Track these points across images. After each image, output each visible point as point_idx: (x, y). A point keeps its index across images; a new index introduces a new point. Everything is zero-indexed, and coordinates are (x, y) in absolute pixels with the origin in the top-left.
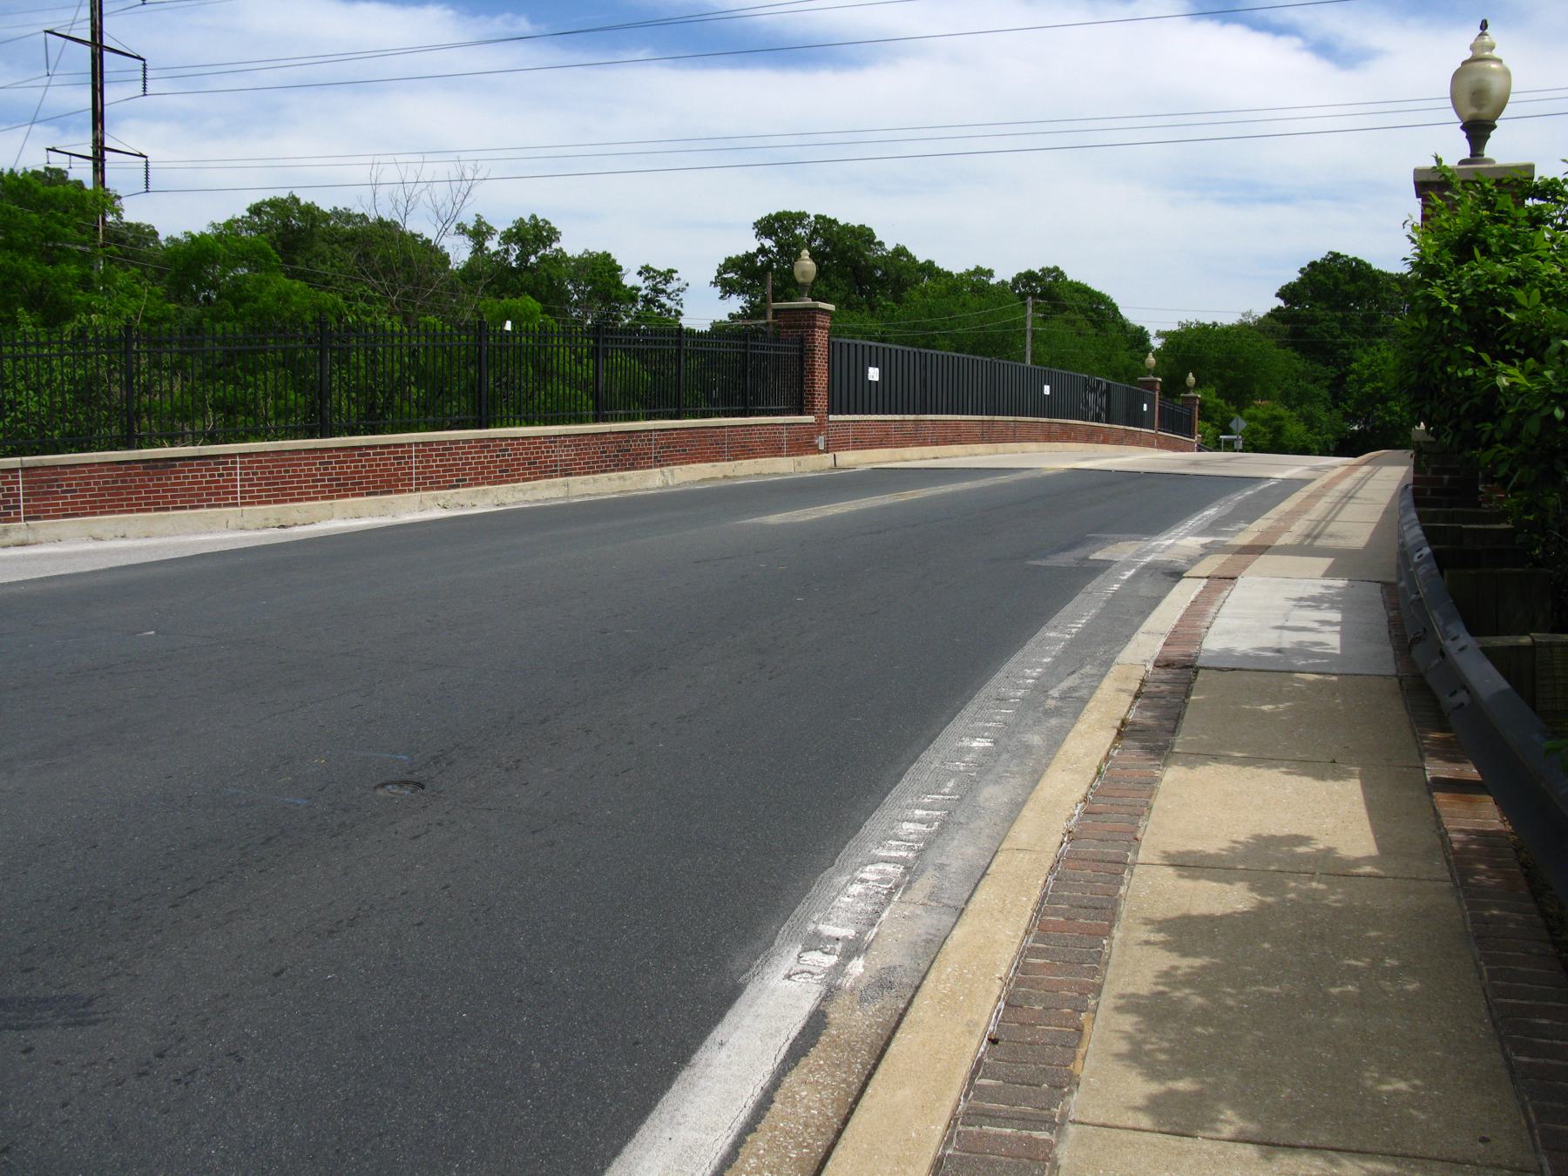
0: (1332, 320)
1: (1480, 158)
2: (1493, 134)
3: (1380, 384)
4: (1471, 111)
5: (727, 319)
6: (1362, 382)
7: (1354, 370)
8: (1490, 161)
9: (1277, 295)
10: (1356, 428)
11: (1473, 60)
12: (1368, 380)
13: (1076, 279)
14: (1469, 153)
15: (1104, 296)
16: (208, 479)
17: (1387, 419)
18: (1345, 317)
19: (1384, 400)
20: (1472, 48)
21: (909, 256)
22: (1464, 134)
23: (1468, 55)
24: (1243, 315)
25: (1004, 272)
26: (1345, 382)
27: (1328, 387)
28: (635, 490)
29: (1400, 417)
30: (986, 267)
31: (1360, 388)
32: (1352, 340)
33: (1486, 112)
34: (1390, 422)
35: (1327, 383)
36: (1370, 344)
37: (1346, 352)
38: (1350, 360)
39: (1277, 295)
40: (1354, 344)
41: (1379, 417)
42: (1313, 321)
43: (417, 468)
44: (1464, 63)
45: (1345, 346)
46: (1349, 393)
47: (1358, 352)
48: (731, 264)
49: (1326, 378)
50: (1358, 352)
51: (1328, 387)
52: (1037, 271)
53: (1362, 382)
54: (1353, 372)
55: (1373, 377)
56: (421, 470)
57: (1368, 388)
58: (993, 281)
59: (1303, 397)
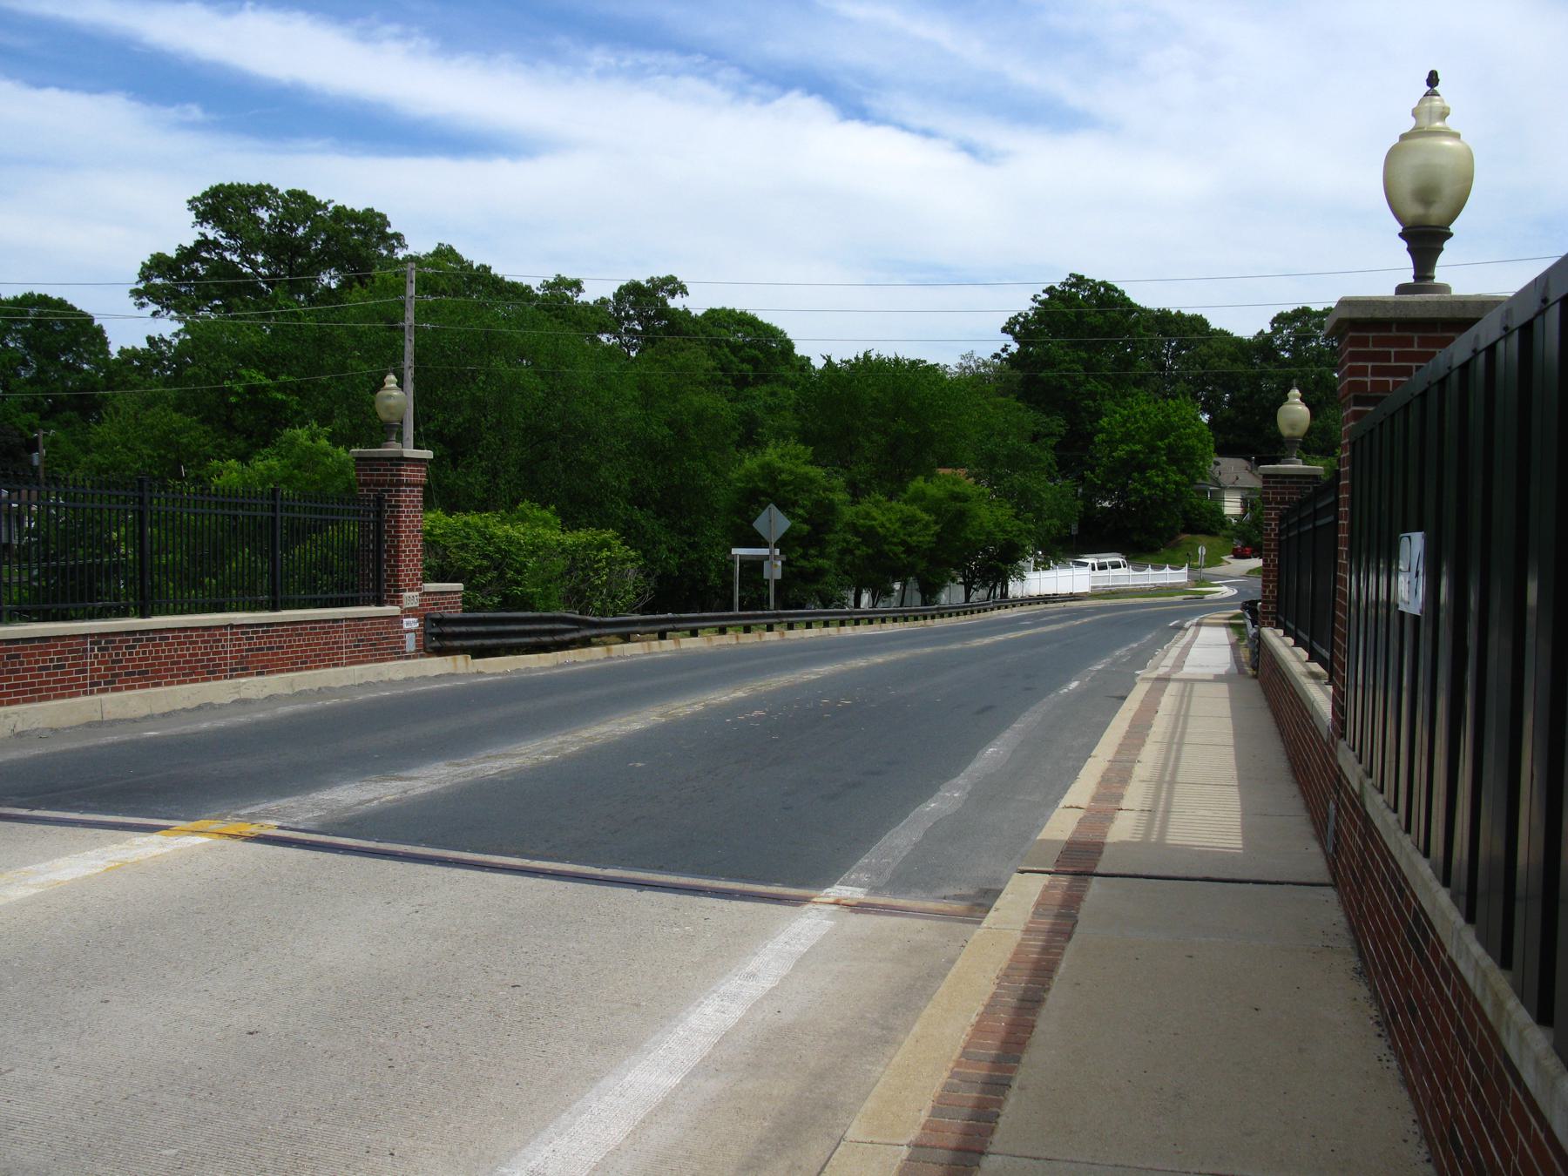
0: (1072, 361)
1: (1428, 283)
2: (1447, 245)
3: (1138, 447)
4: (1414, 210)
5: (146, 346)
6: (1112, 443)
7: (1103, 428)
8: (1444, 288)
9: (1004, 330)
10: (1106, 504)
11: (1416, 133)
12: (1122, 441)
13: (845, 352)
14: (1412, 272)
15: (775, 329)
16: (10, 667)
17: (1146, 493)
18: (1090, 358)
19: (1142, 468)
20: (1415, 113)
21: (458, 259)
22: (1404, 245)
23: (1409, 124)
24: (963, 357)
25: (597, 289)
26: (1093, 443)
27: (1054, 448)
28: (588, 662)
29: (1163, 490)
30: (570, 275)
31: (1111, 452)
32: (1101, 388)
33: (1436, 214)
34: (1150, 497)
35: (1053, 441)
36: (1124, 396)
37: (1091, 403)
38: (1098, 415)
39: (1004, 330)
40: (1103, 394)
41: (1137, 491)
42: (1050, 363)
43: (226, 640)
44: (1403, 137)
45: (1092, 395)
46: (1098, 459)
47: (1109, 405)
48: (159, 264)
49: (1052, 434)
50: (1109, 405)
51: (1054, 448)
52: (644, 283)
53: (1112, 443)
54: (1102, 430)
55: (1128, 437)
56: (223, 638)
57: (1121, 452)
58: (582, 298)
59: (1016, 460)
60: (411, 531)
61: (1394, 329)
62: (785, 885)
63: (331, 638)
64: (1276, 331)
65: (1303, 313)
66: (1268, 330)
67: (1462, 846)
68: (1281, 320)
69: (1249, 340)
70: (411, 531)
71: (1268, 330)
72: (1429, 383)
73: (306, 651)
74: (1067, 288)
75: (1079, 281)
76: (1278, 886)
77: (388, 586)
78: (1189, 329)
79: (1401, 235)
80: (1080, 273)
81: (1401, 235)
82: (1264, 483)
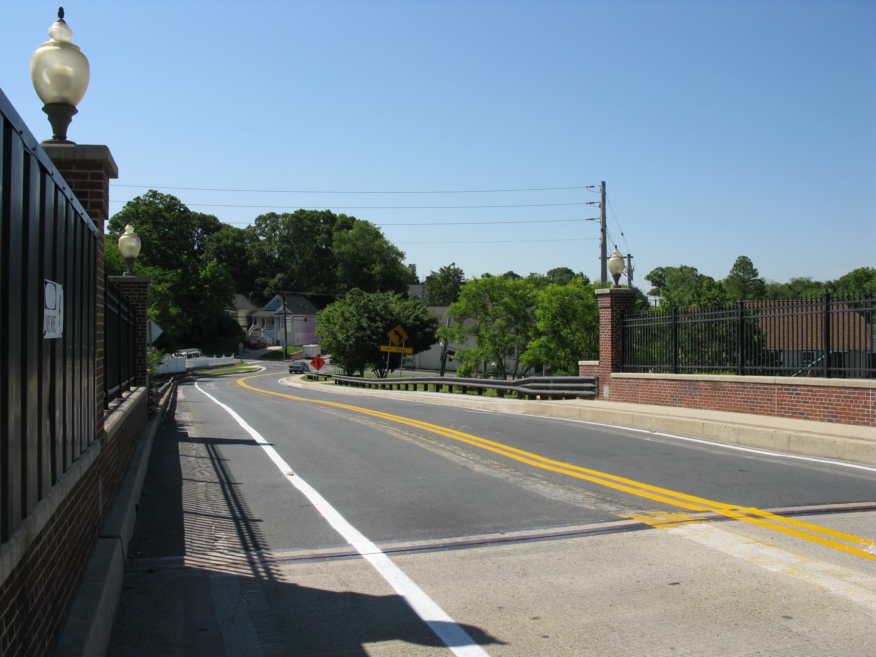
22: (46, 116)
60: (605, 346)
61: (89, 192)
62: (8, 611)
63: (721, 393)
64: (259, 225)
65: (273, 215)
66: (253, 225)
67: (399, 419)
68: (261, 219)
69: (244, 230)
70: (605, 346)
71: (253, 225)
72: (88, 224)
73: (734, 401)
74: (147, 198)
75: (155, 194)
76: (740, 422)
77: (617, 359)
78: (210, 224)
79: (44, 109)
80: (155, 190)
81: (44, 109)
82: (145, 312)
